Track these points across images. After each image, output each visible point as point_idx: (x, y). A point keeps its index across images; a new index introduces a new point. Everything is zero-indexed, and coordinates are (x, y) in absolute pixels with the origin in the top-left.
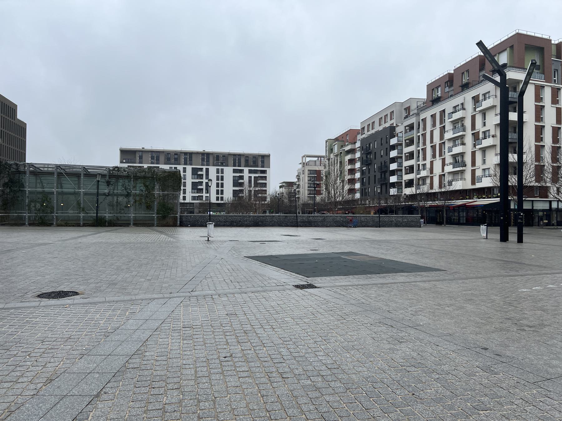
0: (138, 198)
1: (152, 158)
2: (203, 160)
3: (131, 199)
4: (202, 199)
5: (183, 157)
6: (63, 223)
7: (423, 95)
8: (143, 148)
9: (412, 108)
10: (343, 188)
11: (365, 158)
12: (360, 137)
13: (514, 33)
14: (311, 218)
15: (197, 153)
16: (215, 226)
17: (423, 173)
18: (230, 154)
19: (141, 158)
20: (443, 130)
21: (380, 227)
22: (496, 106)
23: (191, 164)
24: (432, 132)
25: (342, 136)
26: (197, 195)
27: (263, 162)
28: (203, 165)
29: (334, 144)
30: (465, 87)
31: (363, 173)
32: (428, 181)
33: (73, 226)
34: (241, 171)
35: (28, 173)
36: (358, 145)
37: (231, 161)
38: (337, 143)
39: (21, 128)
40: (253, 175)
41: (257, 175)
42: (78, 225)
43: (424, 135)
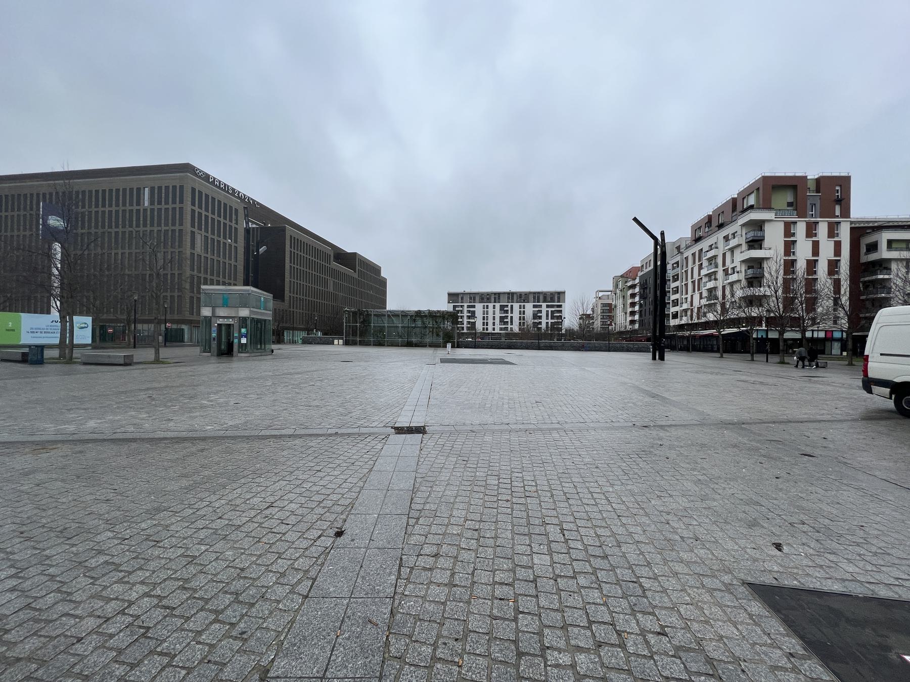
1: (470, 298)
2: (508, 298)
3: (427, 330)
7: (688, 234)
9: (681, 247)
10: (626, 320)
11: (642, 293)
12: (640, 274)
13: (760, 176)
15: (504, 293)
16: (453, 347)
17: (685, 306)
18: (530, 293)
19: (462, 298)
20: (701, 267)
21: (609, 351)
22: (741, 244)
24: (692, 269)
25: (626, 273)
26: (504, 326)
28: (508, 302)
30: (721, 226)
31: (641, 306)
32: (689, 313)
34: (541, 306)
36: (637, 281)
39: (383, 283)
40: (550, 310)
41: (553, 309)
43: (686, 272)
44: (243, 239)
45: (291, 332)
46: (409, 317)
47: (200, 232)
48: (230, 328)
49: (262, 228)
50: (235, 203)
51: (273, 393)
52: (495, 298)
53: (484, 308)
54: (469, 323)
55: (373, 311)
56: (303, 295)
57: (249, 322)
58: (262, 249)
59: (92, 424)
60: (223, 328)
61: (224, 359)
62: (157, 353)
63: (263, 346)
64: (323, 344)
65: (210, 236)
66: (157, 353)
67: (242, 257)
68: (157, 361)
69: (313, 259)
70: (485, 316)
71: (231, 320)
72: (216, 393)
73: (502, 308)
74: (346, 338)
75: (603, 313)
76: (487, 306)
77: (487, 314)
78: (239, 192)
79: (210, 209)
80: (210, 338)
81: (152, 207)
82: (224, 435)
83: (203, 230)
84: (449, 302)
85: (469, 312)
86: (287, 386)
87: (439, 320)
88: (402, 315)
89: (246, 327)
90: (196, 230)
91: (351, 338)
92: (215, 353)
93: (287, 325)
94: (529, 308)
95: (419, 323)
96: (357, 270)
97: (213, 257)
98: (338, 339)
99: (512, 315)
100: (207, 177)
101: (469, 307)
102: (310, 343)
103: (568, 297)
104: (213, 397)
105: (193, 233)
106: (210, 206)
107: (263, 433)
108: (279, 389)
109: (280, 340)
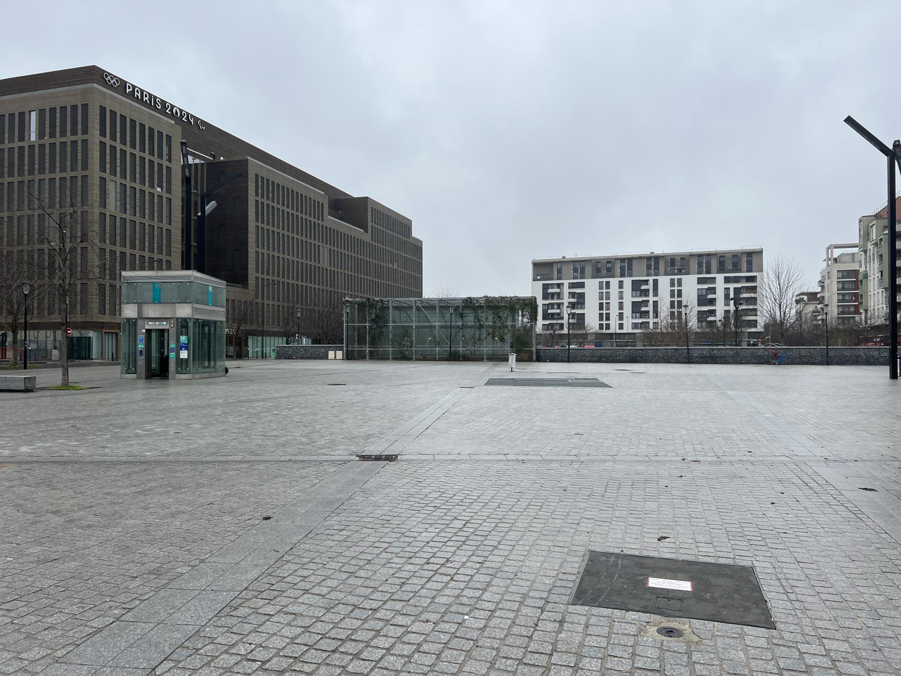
0: (490, 330)
1: (575, 270)
2: (649, 267)
3: (484, 331)
4: (648, 328)
5: (746, 259)
6: (421, 357)
8: (563, 257)
14: (715, 352)
15: (640, 258)
18: (692, 255)
19: (560, 271)
23: (631, 276)
26: (640, 321)
27: (750, 263)
28: (648, 275)
29: (870, 225)
33: (430, 360)
35: (391, 307)
37: (694, 265)
38: (874, 222)
39: (417, 248)
40: (732, 286)
42: (434, 359)
44: (180, 185)
45: (260, 338)
46: (452, 311)
47: (113, 177)
48: (163, 336)
49: (210, 165)
50: (166, 125)
51: (223, 422)
52: (622, 269)
53: (601, 288)
54: (572, 315)
55: (392, 301)
56: (278, 276)
57: (191, 325)
58: (210, 206)
59: (24, 449)
60: (154, 335)
61: (156, 382)
62: (66, 374)
63: (212, 363)
64: (310, 358)
65: (129, 183)
66: (66, 374)
67: (179, 215)
68: (66, 385)
69: (290, 210)
70: (604, 301)
71: (165, 323)
72: (153, 422)
73: (636, 285)
74: (347, 347)
75: (843, 289)
76: (608, 283)
77: (608, 298)
78: (173, 106)
79: (128, 138)
80: (135, 353)
81: (42, 142)
82: (166, 460)
83: (118, 175)
84: (535, 279)
85: (572, 295)
86: (241, 415)
87: (505, 314)
88: (440, 307)
89: (187, 334)
90: (107, 175)
91: (356, 348)
92: (143, 376)
93: (254, 327)
94: (690, 285)
95: (470, 319)
96: (370, 228)
97: (133, 218)
98: (335, 349)
99: (656, 299)
100: (122, 85)
101: (572, 286)
102: (290, 358)
103: (768, 261)
104: (148, 427)
105: (103, 180)
106: (128, 134)
107: (208, 459)
108: (231, 419)
109: (241, 354)
